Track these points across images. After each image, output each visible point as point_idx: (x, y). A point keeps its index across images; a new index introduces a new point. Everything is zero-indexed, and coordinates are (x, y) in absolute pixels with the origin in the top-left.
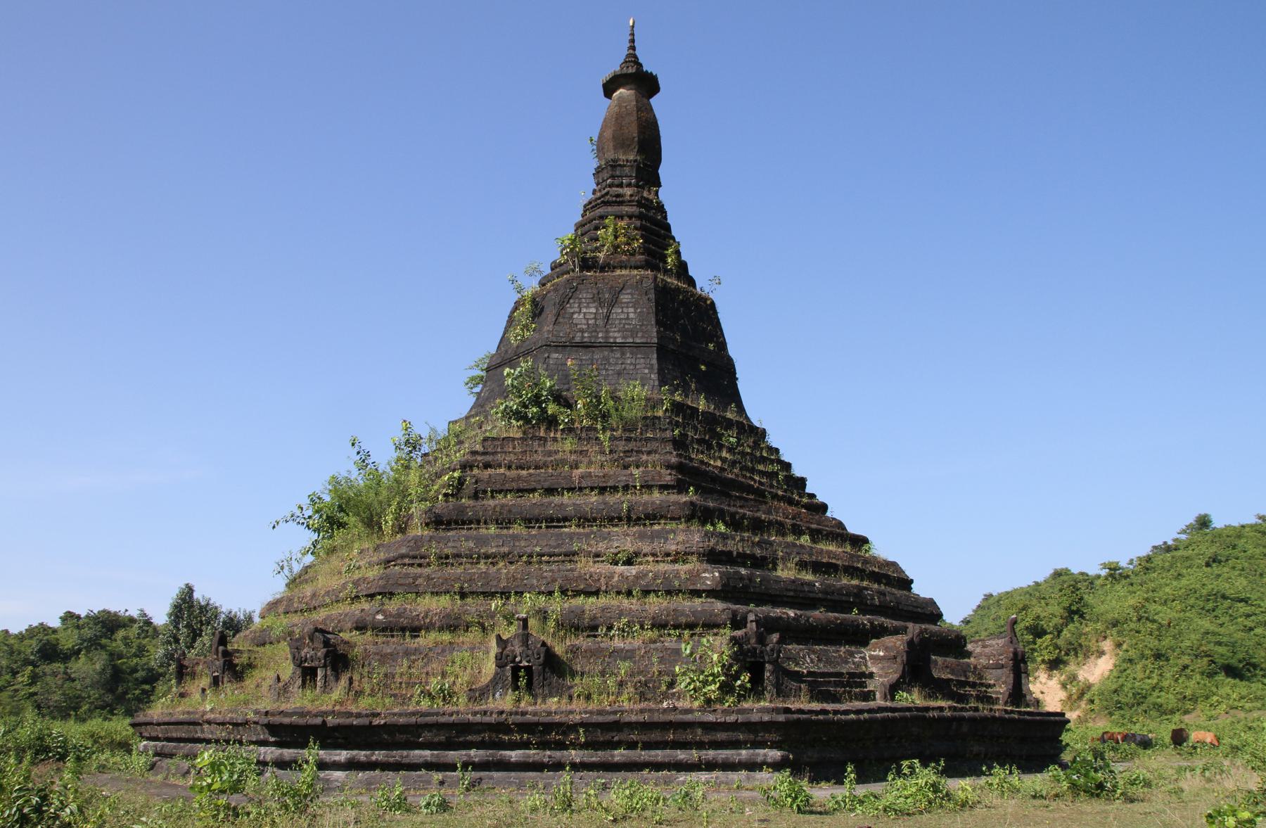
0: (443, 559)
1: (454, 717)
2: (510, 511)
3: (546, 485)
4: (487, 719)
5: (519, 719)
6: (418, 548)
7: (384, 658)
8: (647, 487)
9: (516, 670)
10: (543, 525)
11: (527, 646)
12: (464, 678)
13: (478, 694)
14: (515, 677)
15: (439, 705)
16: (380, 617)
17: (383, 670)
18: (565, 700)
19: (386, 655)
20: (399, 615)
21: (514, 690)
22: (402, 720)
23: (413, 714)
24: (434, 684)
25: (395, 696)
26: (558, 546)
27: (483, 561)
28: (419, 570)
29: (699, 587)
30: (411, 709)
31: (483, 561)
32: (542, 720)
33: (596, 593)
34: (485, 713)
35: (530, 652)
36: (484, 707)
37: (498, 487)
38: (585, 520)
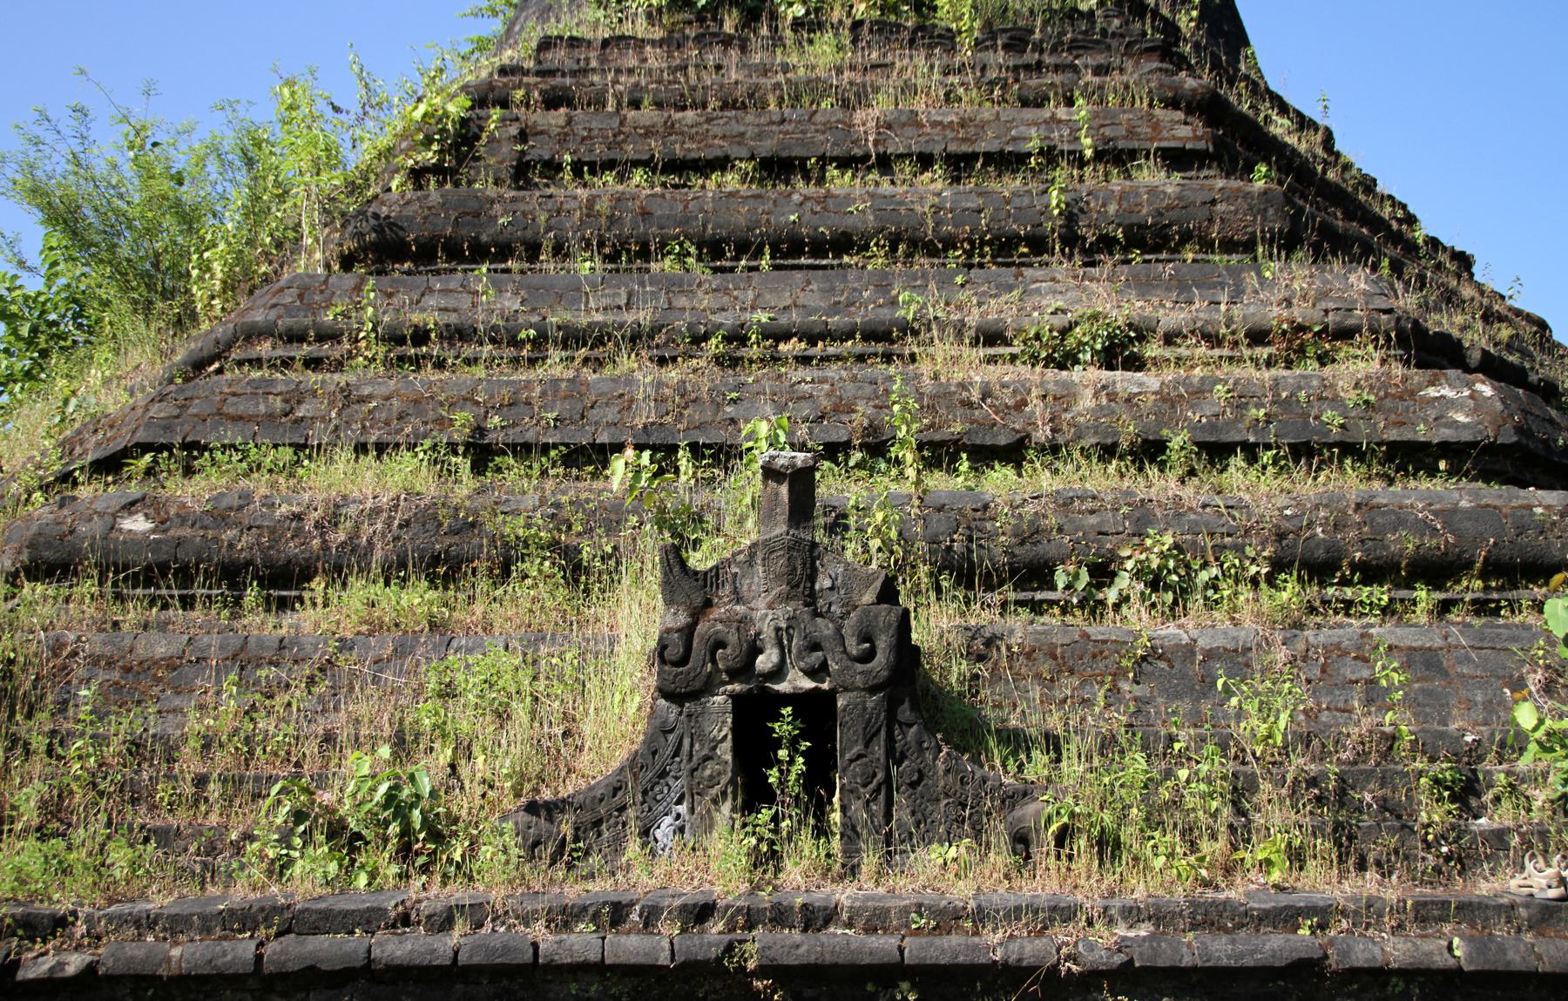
0: (406, 344)
1: (458, 934)
2: (645, 214)
3: (766, 147)
4: (629, 946)
5: (795, 945)
6: (313, 309)
7: (131, 680)
8: (1116, 157)
9: (754, 712)
10: (765, 262)
11: (811, 598)
12: (500, 760)
13: (565, 825)
14: (753, 749)
15: (379, 877)
16: (137, 524)
17: (122, 727)
18: (1000, 858)
19: (147, 666)
20: (219, 516)
21: (749, 807)
22: (182, 954)
23: (244, 919)
24: (358, 779)
25: (165, 837)
26: (835, 308)
27: (555, 354)
28: (313, 378)
29: (1422, 432)
30: (240, 894)
31: (555, 354)
32: (917, 950)
33: (1014, 454)
34: (617, 913)
35: (825, 628)
36: (601, 888)
37: (599, 152)
38: (912, 242)
